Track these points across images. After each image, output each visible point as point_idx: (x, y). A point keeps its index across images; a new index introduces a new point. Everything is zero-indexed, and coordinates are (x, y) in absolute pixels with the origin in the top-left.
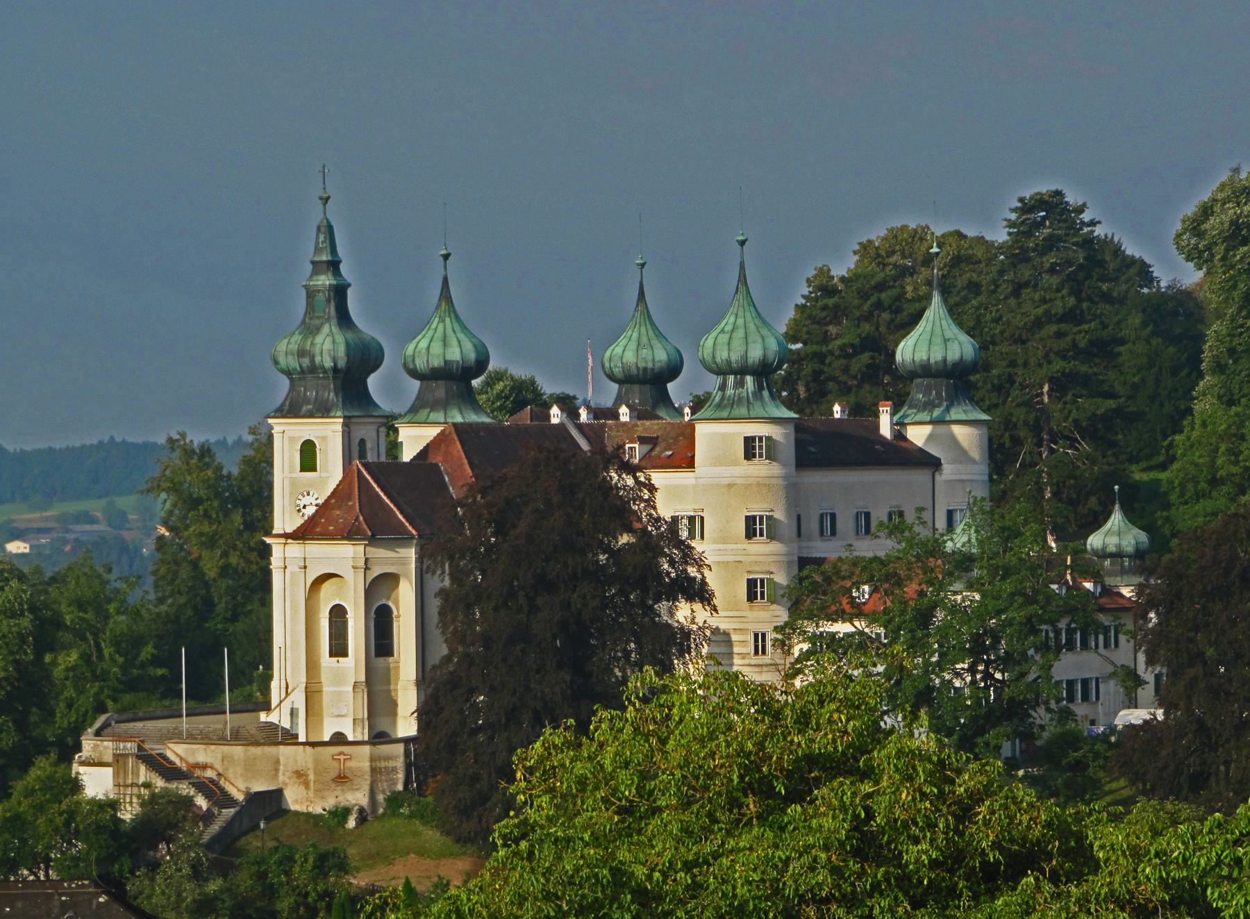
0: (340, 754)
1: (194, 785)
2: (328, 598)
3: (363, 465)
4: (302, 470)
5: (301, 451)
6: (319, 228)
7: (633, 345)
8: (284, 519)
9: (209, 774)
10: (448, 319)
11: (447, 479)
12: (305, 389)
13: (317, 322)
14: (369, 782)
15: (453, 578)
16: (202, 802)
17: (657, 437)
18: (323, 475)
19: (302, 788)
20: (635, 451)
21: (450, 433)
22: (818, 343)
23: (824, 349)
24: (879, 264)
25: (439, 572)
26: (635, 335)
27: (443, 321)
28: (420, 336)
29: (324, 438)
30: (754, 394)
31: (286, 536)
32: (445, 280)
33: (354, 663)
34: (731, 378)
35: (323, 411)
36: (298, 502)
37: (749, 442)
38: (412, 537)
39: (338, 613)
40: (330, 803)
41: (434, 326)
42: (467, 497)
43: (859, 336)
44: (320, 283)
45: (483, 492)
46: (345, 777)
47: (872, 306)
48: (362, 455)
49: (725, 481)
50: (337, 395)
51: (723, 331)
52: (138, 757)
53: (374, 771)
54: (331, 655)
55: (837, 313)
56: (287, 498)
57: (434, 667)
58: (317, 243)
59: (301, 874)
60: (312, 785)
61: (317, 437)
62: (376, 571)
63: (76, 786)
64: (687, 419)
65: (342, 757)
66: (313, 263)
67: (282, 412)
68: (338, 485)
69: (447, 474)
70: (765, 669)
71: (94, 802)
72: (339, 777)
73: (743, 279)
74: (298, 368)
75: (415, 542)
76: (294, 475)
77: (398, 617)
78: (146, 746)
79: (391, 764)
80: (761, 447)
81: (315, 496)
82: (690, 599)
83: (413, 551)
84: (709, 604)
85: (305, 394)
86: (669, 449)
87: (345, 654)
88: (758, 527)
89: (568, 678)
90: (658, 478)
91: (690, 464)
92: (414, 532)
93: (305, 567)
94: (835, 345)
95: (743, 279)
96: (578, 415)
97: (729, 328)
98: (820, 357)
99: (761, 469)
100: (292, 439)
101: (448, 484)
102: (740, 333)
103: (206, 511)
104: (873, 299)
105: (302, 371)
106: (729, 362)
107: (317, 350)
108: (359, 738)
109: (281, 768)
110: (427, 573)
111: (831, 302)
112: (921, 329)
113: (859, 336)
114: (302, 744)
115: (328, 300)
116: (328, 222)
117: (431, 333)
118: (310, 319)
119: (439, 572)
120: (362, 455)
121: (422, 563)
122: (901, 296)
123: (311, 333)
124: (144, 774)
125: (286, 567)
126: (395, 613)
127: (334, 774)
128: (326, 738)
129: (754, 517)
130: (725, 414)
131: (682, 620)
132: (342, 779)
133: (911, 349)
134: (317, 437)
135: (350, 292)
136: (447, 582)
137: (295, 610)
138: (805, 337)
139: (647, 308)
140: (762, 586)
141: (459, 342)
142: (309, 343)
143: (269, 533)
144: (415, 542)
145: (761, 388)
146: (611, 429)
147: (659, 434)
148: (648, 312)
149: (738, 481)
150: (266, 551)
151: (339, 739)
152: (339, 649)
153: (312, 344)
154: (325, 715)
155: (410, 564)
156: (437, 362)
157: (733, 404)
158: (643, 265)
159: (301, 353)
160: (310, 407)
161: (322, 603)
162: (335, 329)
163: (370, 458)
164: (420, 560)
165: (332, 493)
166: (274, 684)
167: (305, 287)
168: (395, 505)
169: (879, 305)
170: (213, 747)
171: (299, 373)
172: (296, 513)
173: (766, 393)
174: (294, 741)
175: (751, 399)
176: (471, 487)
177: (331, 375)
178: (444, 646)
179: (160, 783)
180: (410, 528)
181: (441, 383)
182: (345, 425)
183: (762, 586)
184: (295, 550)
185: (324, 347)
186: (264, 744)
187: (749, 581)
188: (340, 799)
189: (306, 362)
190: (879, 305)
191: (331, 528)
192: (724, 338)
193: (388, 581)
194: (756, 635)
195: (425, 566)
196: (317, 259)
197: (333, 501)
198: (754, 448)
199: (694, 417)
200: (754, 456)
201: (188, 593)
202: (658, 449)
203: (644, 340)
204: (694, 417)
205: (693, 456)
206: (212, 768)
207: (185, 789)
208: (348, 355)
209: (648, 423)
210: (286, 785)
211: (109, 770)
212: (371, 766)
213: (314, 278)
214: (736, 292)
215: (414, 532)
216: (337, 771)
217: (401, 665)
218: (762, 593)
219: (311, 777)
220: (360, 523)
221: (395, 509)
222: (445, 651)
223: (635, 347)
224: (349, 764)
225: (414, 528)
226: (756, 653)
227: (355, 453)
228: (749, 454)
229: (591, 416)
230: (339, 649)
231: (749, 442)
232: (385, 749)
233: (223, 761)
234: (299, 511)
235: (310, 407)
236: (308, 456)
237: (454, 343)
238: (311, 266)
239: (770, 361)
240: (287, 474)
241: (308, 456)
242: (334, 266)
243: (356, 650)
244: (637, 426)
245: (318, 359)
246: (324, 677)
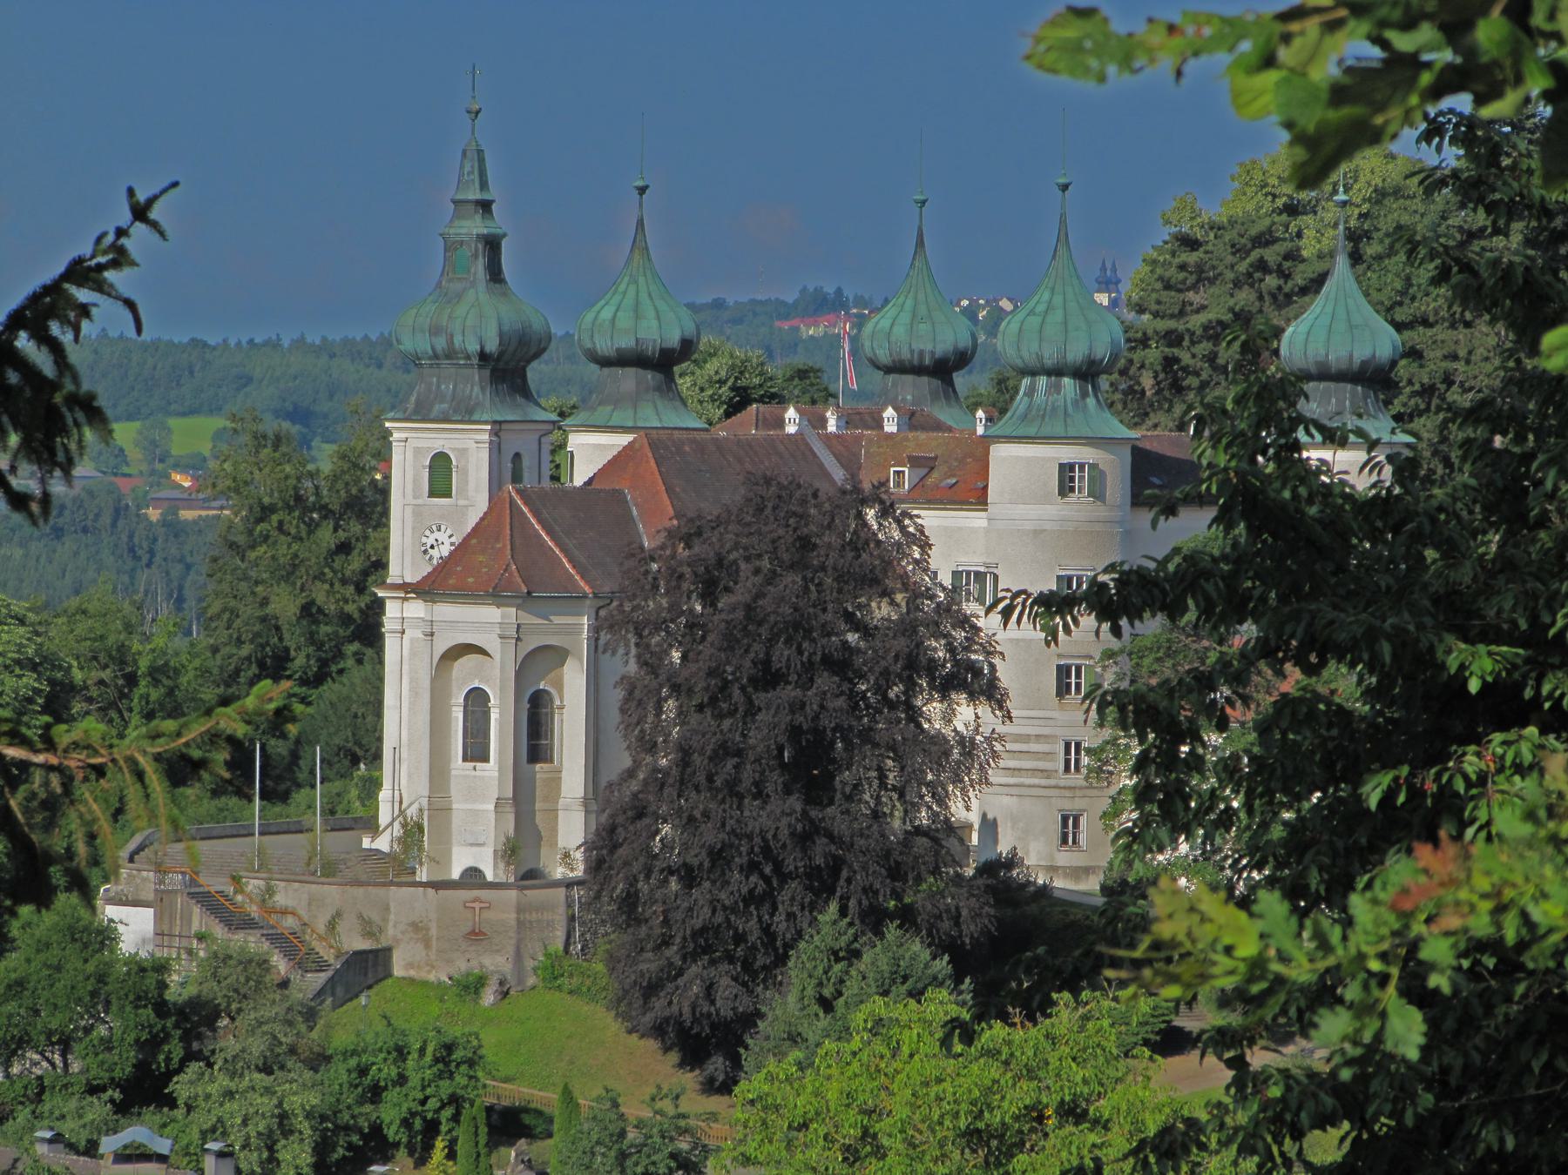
0: (476, 900)
1: (269, 937)
3: (518, 491)
4: (432, 494)
6: (464, 153)
7: (905, 318)
8: (403, 564)
9: (290, 922)
10: (641, 280)
11: (635, 512)
13: (458, 286)
14: (513, 942)
15: (643, 663)
16: (280, 964)
17: (936, 458)
19: (420, 946)
20: (900, 478)
21: (642, 447)
22: (1172, 316)
23: (1181, 327)
24: (1266, 195)
25: (621, 651)
26: (909, 303)
27: (636, 282)
28: (602, 302)
29: (463, 452)
30: (1075, 403)
31: (404, 587)
32: (640, 224)
33: (493, 773)
34: (1042, 381)
35: (463, 413)
36: (424, 540)
37: (1066, 470)
38: (585, 597)
39: (477, 699)
40: (461, 966)
41: (622, 287)
42: (663, 547)
43: (1231, 310)
44: (464, 231)
45: (688, 541)
46: (481, 933)
47: (1251, 265)
48: (517, 477)
49: (1029, 526)
50: (483, 389)
51: (1032, 312)
52: (192, 895)
53: (520, 923)
54: (465, 759)
55: (1202, 276)
56: (408, 532)
57: (610, 785)
58: (461, 175)
59: (418, 1070)
60: (434, 943)
61: (453, 450)
62: (532, 643)
63: (106, 936)
64: (980, 430)
65: (477, 905)
66: (455, 202)
68: (482, 519)
69: (637, 505)
70: (1078, 793)
71: (132, 960)
72: (473, 932)
76: (420, 501)
77: (562, 708)
78: (202, 880)
79: (547, 916)
80: (1081, 478)
81: (449, 532)
82: (973, 697)
83: (585, 620)
84: (1001, 708)
85: (438, 386)
86: (953, 476)
87: (486, 759)
88: (1073, 680)
89: (798, 807)
90: (931, 519)
91: (979, 499)
92: (587, 589)
93: (432, 634)
94: (1196, 322)
96: (824, 421)
97: (1041, 308)
98: (1173, 339)
99: (1079, 505)
101: (637, 519)
102: (1058, 316)
103: (281, 523)
104: (1255, 255)
105: (436, 356)
106: (1040, 357)
108: (502, 878)
109: (392, 917)
110: (604, 652)
111: (1192, 258)
112: (1318, 310)
113: (1231, 310)
114: (421, 884)
115: (476, 256)
117: (617, 298)
118: (450, 280)
119: (621, 651)
120: (517, 477)
121: (597, 639)
122: (1293, 256)
123: (449, 302)
124: (199, 919)
125: (403, 632)
126: (557, 702)
127: (467, 928)
128: (456, 874)
129: (1068, 668)
130: (1032, 431)
131: (961, 728)
132: (476, 935)
133: (1302, 337)
135: (504, 243)
136: (632, 667)
137: (414, 692)
138: (1154, 307)
139: (927, 263)
140: (1078, 676)
141: (657, 312)
142: (446, 317)
143: (382, 584)
144: (588, 602)
145: (1084, 395)
146: (870, 441)
147: (939, 453)
148: (929, 269)
149: (1048, 526)
150: (378, 606)
151: (472, 876)
152: (476, 751)
154: (455, 837)
155: (580, 633)
156: (626, 342)
157: (1043, 416)
158: (923, 202)
159: (435, 331)
160: (445, 406)
161: (454, 689)
162: (483, 296)
163: (529, 480)
164: (596, 630)
165: (474, 530)
166: (384, 795)
168: (562, 550)
169: (1262, 266)
170: (296, 885)
171: (430, 358)
173: (1091, 401)
174: (409, 879)
175: (1070, 409)
176: (671, 534)
177: (475, 361)
178: (627, 754)
179: (219, 931)
180: (582, 584)
181: (631, 372)
182: (495, 433)
183: (1078, 676)
184: (416, 609)
186: (368, 884)
187: (1059, 667)
188: (474, 963)
189: (441, 343)
190: (1262, 266)
191: (471, 580)
192: (1035, 321)
193: (549, 657)
194: (1068, 746)
195: (602, 642)
196: (460, 197)
197: (474, 541)
198: (1072, 479)
199: (994, 431)
200: (1072, 489)
201: (252, 641)
202: (935, 475)
203: (922, 310)
204: (994, 431)
205: (985, 488)
206: (293, 914)
207: (253, 943)
208: (501, 335)
209: (922, 436)
210: (398, 941)
211: (149, 913)
212: (518, 920)
213: (456, 223)
214: (1054, 257)
215: (587, 589)
216: (470, 924)
217: (564, 774)
218: (1078, 686)
219: (434, 932)
220: (511, 574)
221: (561, 556)
222: (627, 762)
223: (908, 321)
224: (486, 914)
225: (587, 582)
226: (1067, 769)
227: (508, 475)
228: (1066, 487)
229: (843, 423)
230: (476, 751)
231: (1066, 470)
232: (534, 895)
233: (309, 904)
234: (425, 552)
235: (445, 406)
236: (440, 475)
237: (651, 313)
239: (1099, 356)
240: (410, 499)
241: (440, 475)
243: (501, 752)
244: (907, 439)
245: (457, 341)
246: (455, 790)
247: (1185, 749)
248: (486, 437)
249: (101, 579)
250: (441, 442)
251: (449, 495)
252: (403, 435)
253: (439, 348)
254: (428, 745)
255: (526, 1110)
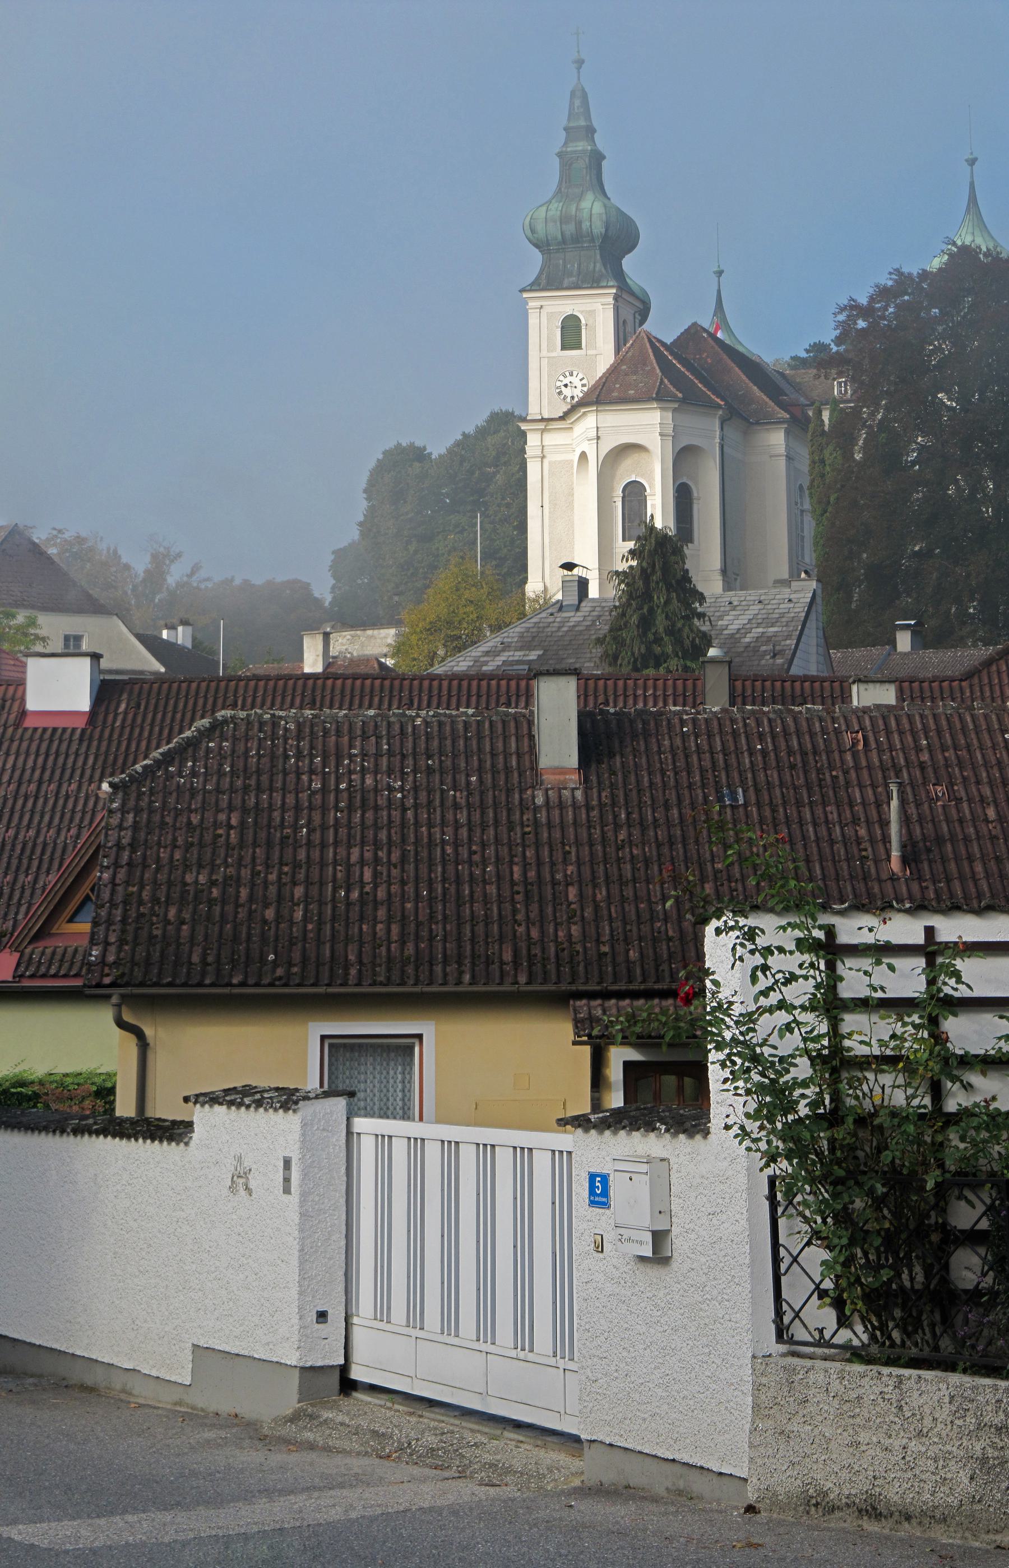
2: (626, 473)
4: (564, 348)
5: (562, 328)
6: (573, 94)
12: (564, 260)
18: (590, 352)
35: (589, 281)
50: (605, 265)
66: (565, 129)
67: (539, 285)
73: (973, 200)
74: (560, 237)
75: (720, 412)
76: (554, 354)
81: (580, 376)
85: (565, 266)
95: (973, 200)
100: (551, 316)
105: (564, 241)
107: (585, 214)
116: (583, 91)
125: (543, 457)
126: (695, 494)
134: (582, 312)
144: (720, 412)
153: (577, 209)
159: (564, 219)
167: (560, 155)
172: (556, 396)
185: (593, 212)
189: (570, 229)
220: (666, 386)
234: (560, 393)
238: (563, 134)
240: (544, 353)
242: (590, 131)
245: (586, 225)
247: (971, 611)
248: (610, 300)
249: (446, 555)
250: (572, 307)
251: (579, 347)
252: (538, 304)
253: (568, 233)
254: (530, 385)
255: (856, 1354)
